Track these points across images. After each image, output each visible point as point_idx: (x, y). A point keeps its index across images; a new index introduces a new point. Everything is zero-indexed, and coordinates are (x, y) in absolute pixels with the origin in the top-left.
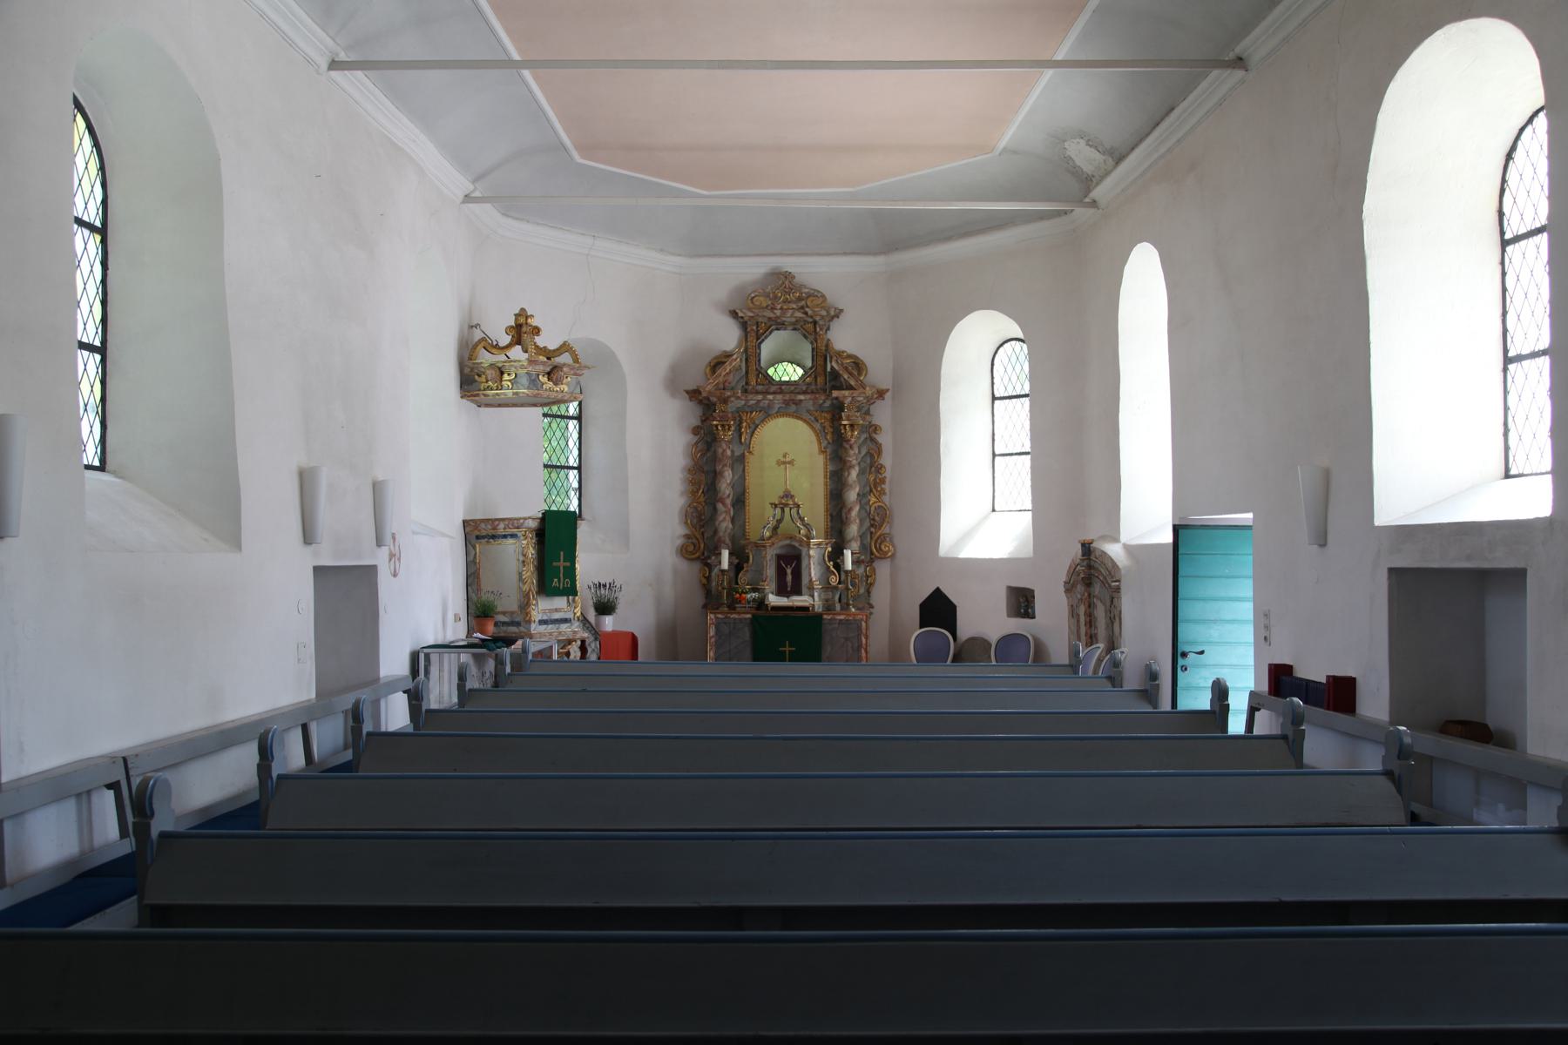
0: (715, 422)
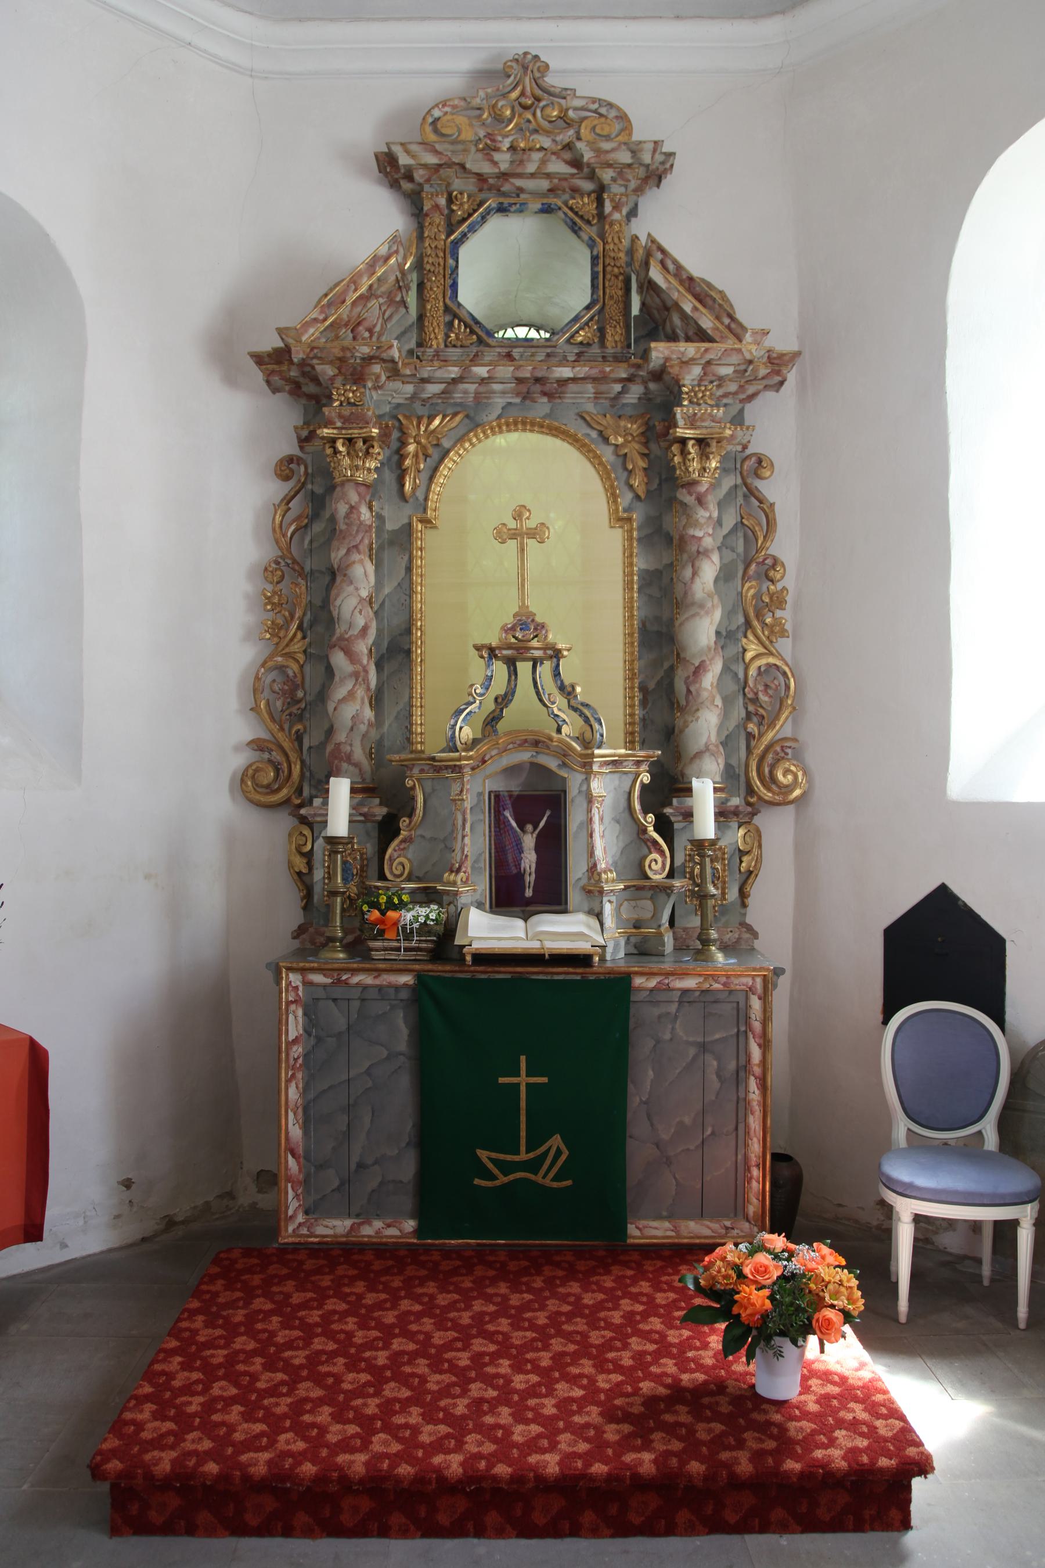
0: (326, 432)
